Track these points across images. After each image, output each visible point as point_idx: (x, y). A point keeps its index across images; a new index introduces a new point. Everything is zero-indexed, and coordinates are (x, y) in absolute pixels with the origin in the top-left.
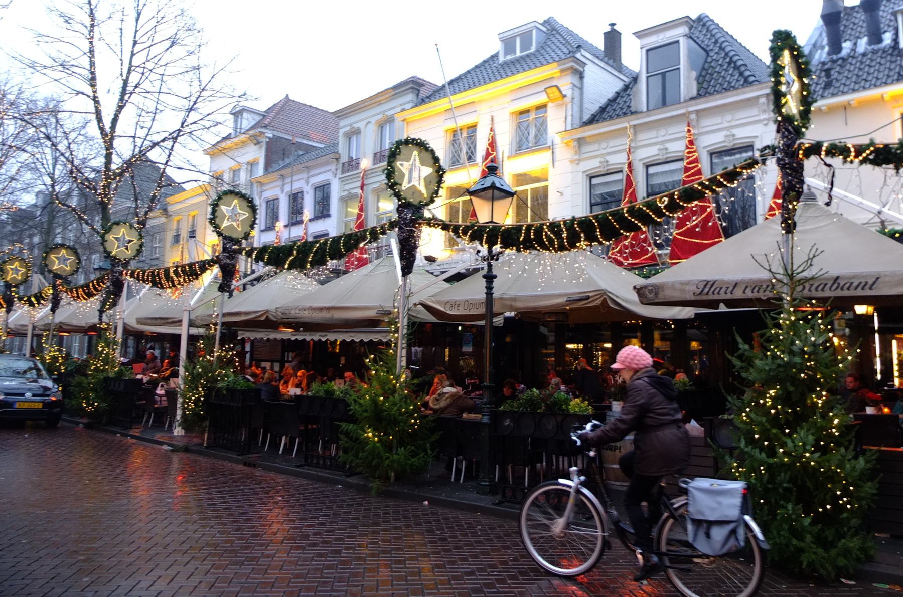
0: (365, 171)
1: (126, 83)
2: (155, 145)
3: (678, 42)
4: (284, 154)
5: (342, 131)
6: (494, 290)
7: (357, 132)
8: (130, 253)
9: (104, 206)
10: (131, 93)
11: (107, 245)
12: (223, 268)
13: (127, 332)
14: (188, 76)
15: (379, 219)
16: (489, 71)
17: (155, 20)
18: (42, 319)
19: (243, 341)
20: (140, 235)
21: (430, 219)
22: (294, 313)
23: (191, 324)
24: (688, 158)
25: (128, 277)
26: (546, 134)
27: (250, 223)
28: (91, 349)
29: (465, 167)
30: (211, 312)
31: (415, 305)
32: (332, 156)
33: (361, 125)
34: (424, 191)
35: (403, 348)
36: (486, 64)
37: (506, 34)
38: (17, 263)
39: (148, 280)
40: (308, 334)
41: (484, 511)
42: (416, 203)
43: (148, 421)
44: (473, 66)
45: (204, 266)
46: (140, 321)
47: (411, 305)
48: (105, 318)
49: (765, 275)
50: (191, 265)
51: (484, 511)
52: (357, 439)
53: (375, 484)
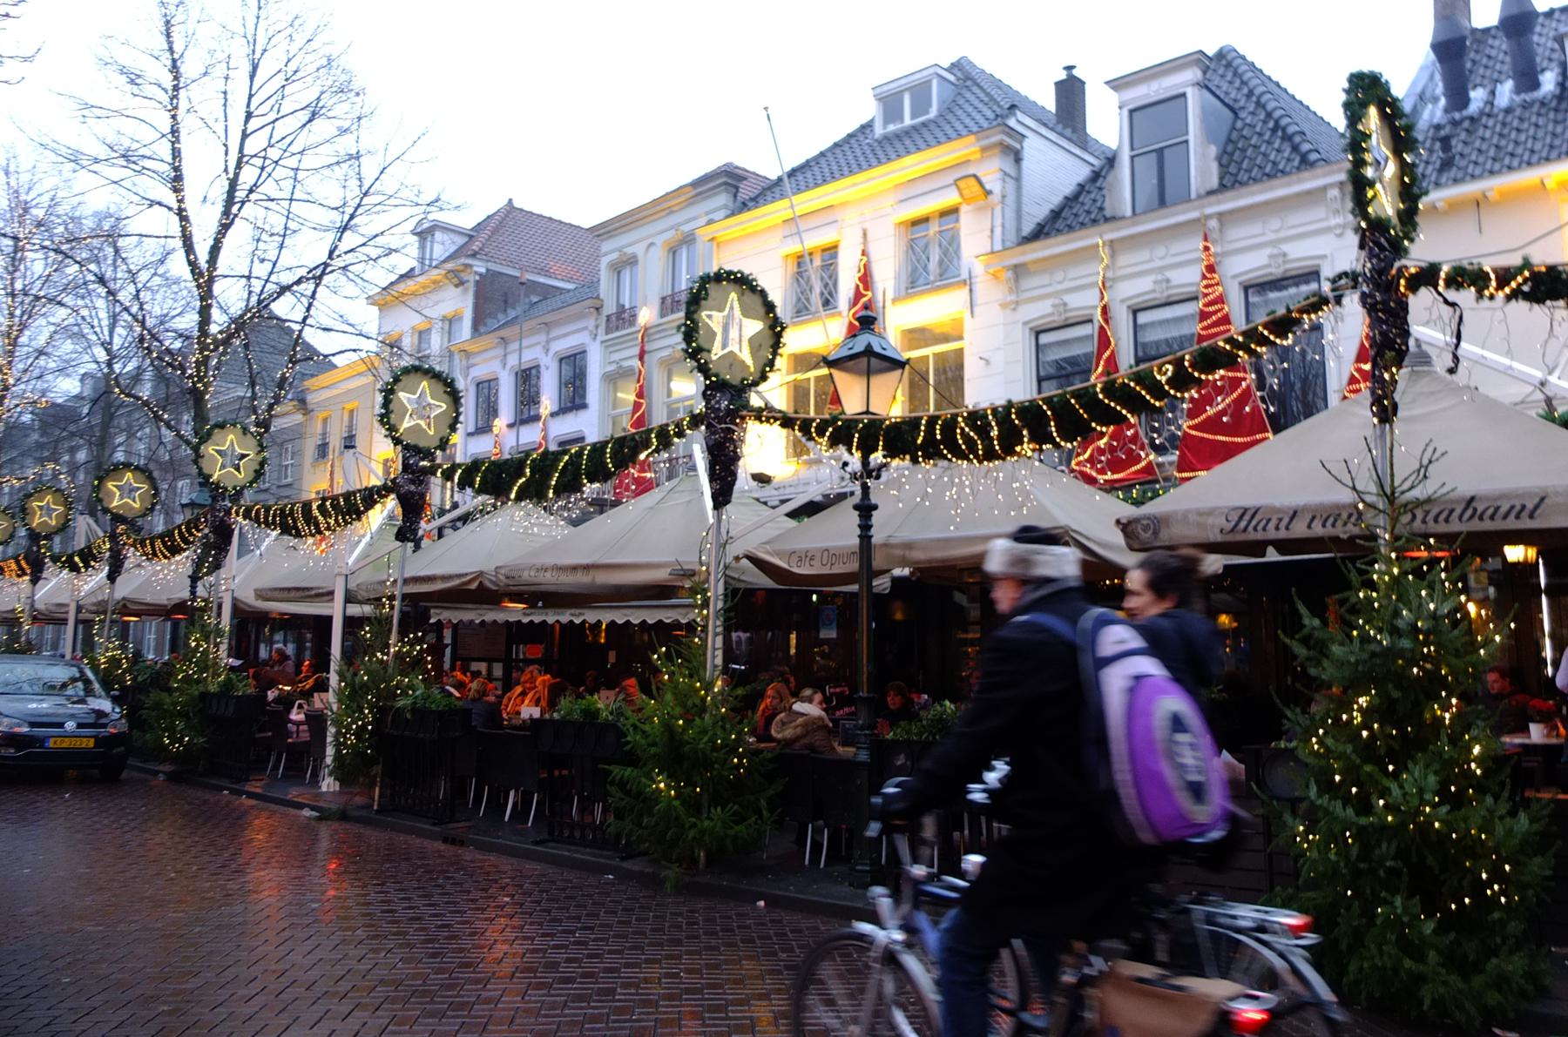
1: (233, 184)
2: (284, 289)
3: (1184, 95)
4: (506, 302)
5: (605, 261)
6: (873, 531)
7: (632, 261)
9: (197, 397)
10: (243, 203)
11: (204, 463)
12: (404, 500)
13: (238, 610)
14: (339, 172)
15: (672, 411)
16: (858, 152)
17: (282, 76)
18: (92, 593)
20: (261, 445)
21: (760, 410)
22: (526, 576)
23: (350, 598)
24: (1206, 295)
25: (240, 519)
27: (450, 421)
29: (818, 319)
31: (737, 559)
32: (589, 302)
33: (638, 249)
34: (749, 361)
35: (716, 634)
37: (886, 88)
42: (736, 382)
43: (276, 768)
45: (371, 497)
46: (261, 594)
47: (729, 559)
49: (1345, 496)
50: (348, 496)
52: (640, 793)
53: (672, 873)
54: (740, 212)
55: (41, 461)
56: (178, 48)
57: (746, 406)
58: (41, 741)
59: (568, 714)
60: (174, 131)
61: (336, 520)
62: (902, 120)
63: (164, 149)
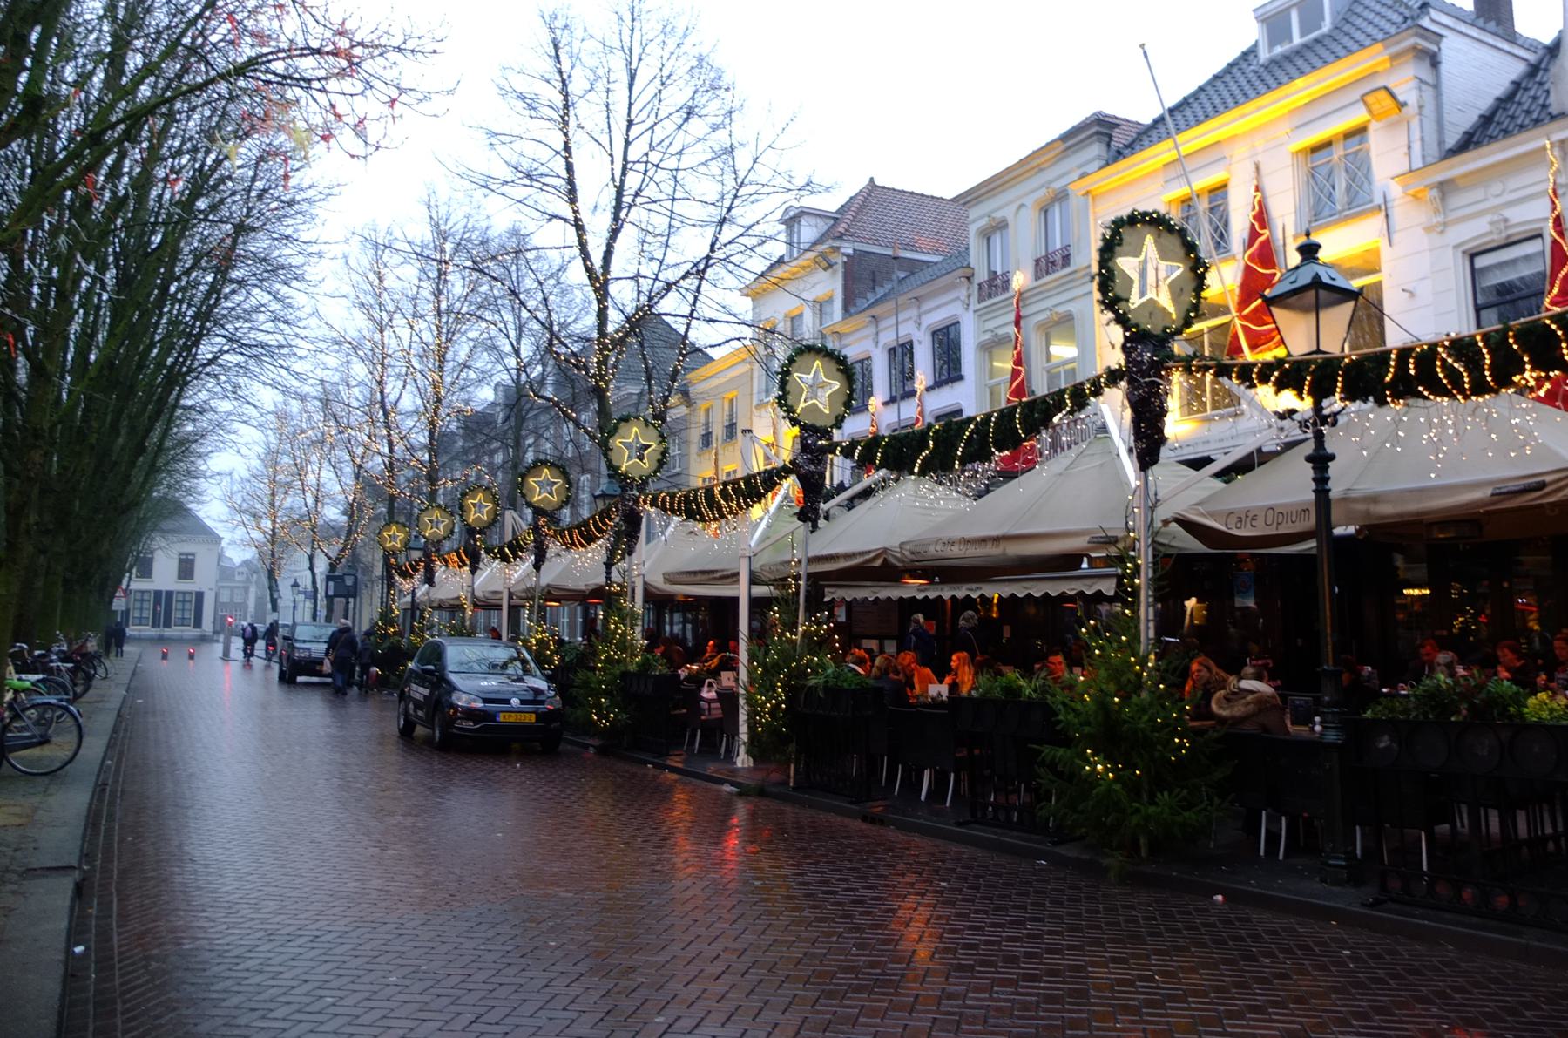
0: (1021, 294)
2: (669, 286)
4: (874, 282)
5: (973, 229)
6: (1330, 484)
7: (1002, 226)
8: (647, 466)
9: (599, 394)
10: (630, 207)
11: (613, 456)
12: (803, 479)
13: (651, 596)
14: (715, 167)
15: (1052, 377)
16: (1243, 81)
17: (658, 81)
18: (521, 580)
19: (831, 605)
20: (662, 436)
22: (932, 551)
23: (754, 580)
25: (647, 507)
26: (1370, 183)
27: (844, 399)
28: (589, 626)
30: (788, 557)
31: (1166, 523)
32: (960, 272)
33: (1008, 213)
34: (1171, 309)
36: (1235, 70)
37: (1269, 8)
38: (480, 495)
39: (679, 509)
40: (946, 587)
41: (1346, 919)
42: (1158, 331)
43: (692, 743)
44: (1209, 76)
45: (771, 479)
46: (668, 578)
48: (615, 576)
50: (748, 479)
51: (1346, 919)
53: (1113, 861)
54: (1115, 160)
55: (467, 464)
56: (566, 67)
57: (1171, 356)
58: (491, 716)
59: (987, 692)
60: (567, 148)
61: (738, 504)
62: (1291, 40)
63: (559, 166)
